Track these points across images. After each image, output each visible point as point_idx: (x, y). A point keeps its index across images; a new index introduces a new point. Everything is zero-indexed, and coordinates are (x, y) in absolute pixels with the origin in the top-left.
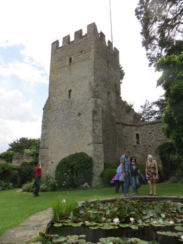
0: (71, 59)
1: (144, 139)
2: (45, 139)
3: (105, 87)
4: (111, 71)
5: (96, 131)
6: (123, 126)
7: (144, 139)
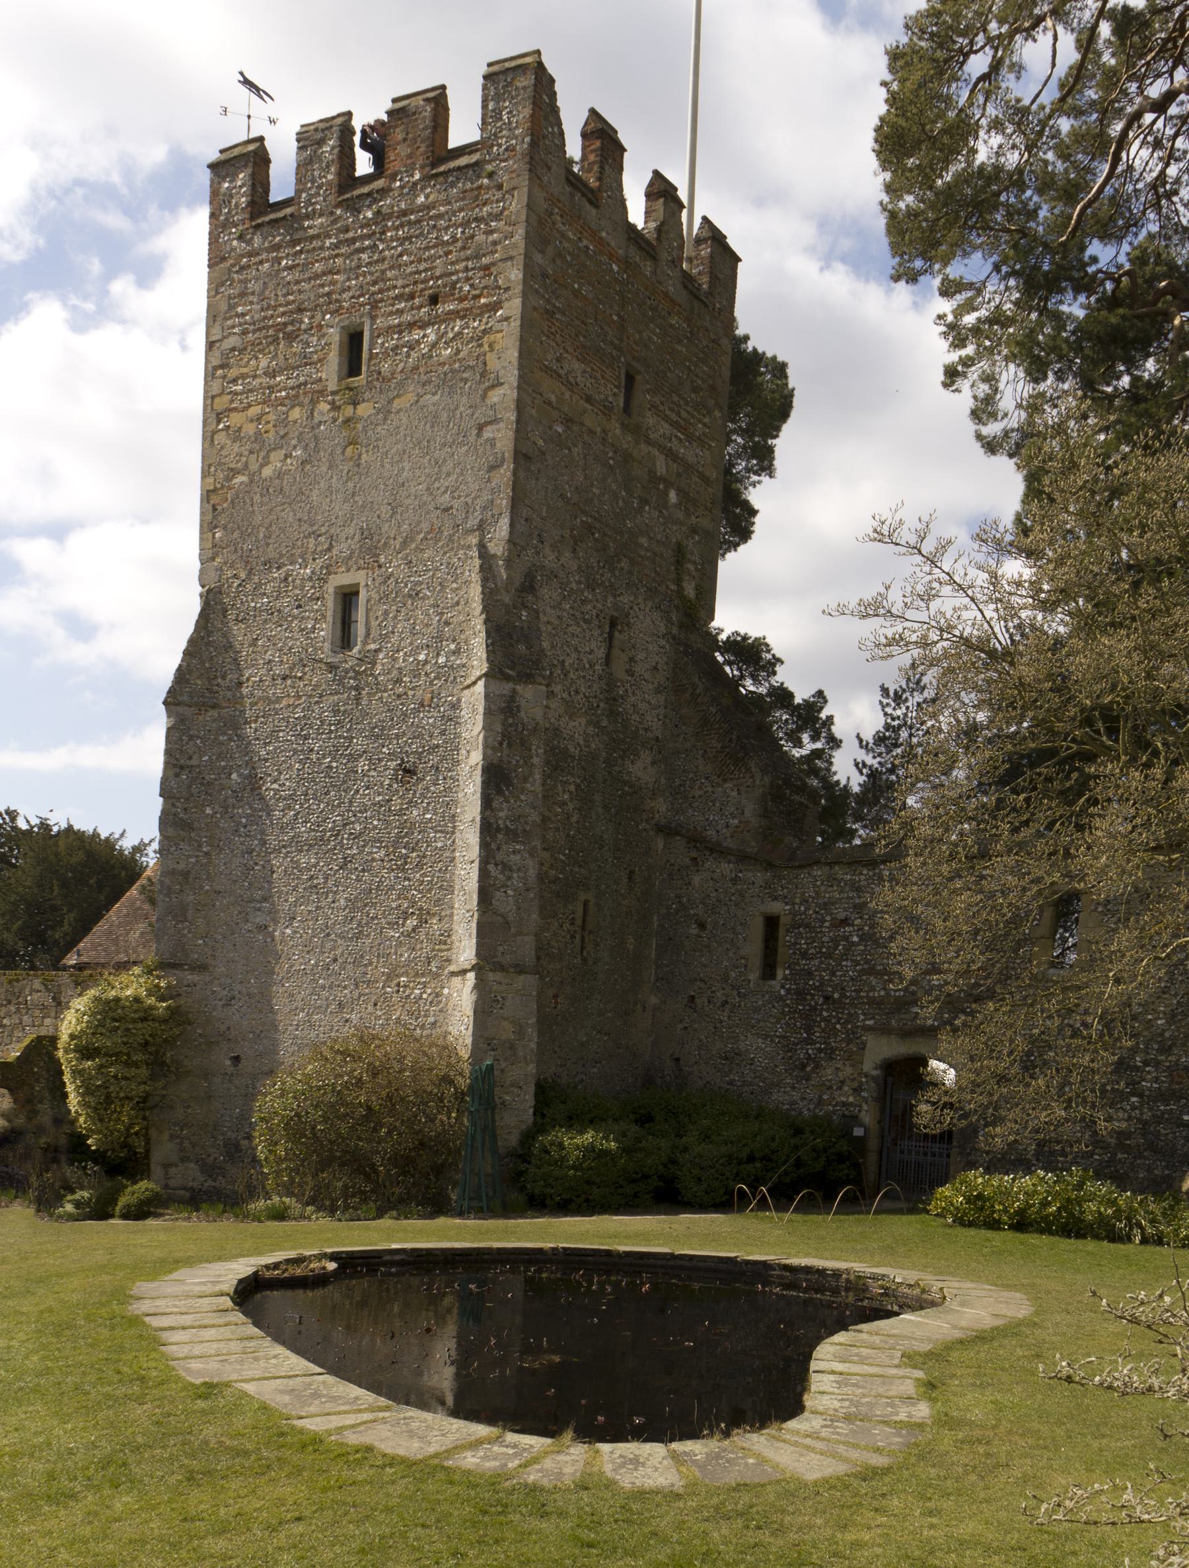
0: (354, 340)
1: (804, 955)
2: (183, 908)
3: (591, 587)
4: (649, 442)
5: (499, 894)
6: (694, 854)
7: (804, 955)
